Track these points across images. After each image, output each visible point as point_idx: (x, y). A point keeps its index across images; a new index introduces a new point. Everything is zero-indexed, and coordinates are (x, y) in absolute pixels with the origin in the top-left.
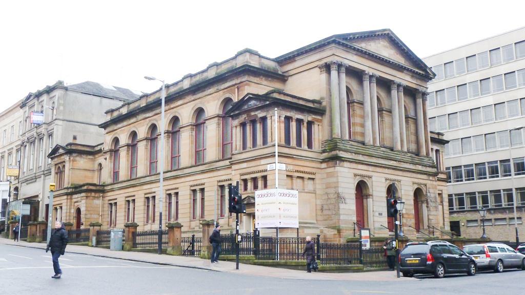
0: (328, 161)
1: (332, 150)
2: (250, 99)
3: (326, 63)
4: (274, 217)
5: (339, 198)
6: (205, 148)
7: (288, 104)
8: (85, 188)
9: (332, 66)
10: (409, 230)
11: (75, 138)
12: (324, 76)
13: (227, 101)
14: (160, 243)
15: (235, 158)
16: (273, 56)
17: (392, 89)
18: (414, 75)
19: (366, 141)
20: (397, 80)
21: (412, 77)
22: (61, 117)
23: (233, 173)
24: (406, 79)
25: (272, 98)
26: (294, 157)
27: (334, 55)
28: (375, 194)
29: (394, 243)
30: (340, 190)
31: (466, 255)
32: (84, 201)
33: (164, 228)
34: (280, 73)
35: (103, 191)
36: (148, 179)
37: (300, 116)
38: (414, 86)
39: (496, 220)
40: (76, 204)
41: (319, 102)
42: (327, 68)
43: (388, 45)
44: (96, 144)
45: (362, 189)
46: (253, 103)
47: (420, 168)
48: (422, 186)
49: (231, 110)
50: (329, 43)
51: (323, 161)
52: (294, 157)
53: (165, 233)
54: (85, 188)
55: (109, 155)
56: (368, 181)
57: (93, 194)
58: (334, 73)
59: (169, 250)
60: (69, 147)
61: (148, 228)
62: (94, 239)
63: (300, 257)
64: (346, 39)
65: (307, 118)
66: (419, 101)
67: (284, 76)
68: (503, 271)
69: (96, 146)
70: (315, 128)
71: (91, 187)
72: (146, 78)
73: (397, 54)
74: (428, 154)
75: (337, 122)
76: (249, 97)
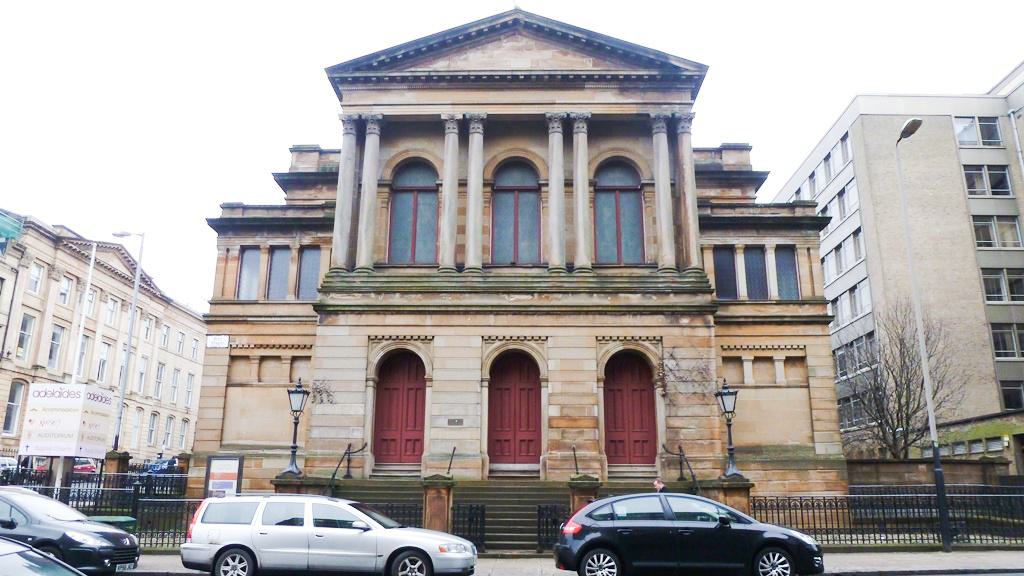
7: (750, 222)
17: (471, 131)
18: (624, 84)
21: (623, 90)
26: (249, 319)
31: (596, 530)
38: (634, 110)
43: (532, 43)
48: (647, 344)
52: (249, 319)
56: (419, 348)
64: (370, 68)
65: (771, 241)
72: (128, 235)
73: (566, 54)
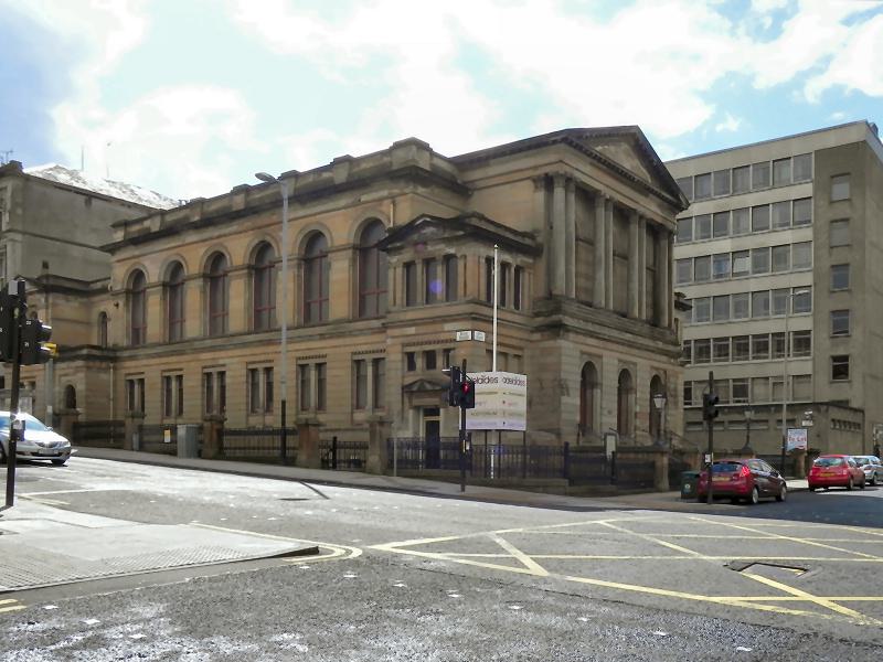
0: (544, 331)
1: (550, 314)
2: (426, 224)
3: (546, 174)
4: (495, 414)
5: (562, 388)
6: (324, 298)
8: (85, 352)
9: (555, 180)
10: (642, 436)
11: (45, 265)
12: (541, 195)
13: (371, 225)
14: (284, 447)
15: (391, 318)
16: (449, 155)
19: (595, 303)
20: (641, 210)
22: (20, 228)
23: (389, 341)
24: (650, 208)
25: (470, 225)
27: (561, 161)
28: (604, 382)
29: (708, 456)
30: (563, 376)
32: (81, 375)
33: (290, 425)
34: (459, 182)
35: (115, 359)
36: (208, 343)
37: (507, 258)
38: (659, 220)
39: (731, 422)
40: (64, 379)
41: (531, 236)
42: (548, 182)
44: (94, 279)
45: (589, 374)
46: (429, 230)
47: (660, 345)
49: (373, 243)
50: (555, 142)
51: (538, 329)
53: (293, 432)
54: (85, 352)
55: (124, 299)
57: (98, 364)
58: (559, 192)
59: (302, 457)
60: (44, 282)
61: (256, 421)
62: (135, 439)
63: (528, 474)
66: (664, 243)
67: (468, 189)
68: (759, 503)
69: (92, 282)
70: (525, 278)
71: (95, 352)
74: (670, 325)
75: (561, 270)
76: (425, 221)
